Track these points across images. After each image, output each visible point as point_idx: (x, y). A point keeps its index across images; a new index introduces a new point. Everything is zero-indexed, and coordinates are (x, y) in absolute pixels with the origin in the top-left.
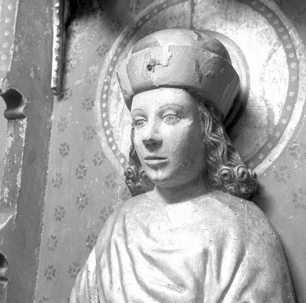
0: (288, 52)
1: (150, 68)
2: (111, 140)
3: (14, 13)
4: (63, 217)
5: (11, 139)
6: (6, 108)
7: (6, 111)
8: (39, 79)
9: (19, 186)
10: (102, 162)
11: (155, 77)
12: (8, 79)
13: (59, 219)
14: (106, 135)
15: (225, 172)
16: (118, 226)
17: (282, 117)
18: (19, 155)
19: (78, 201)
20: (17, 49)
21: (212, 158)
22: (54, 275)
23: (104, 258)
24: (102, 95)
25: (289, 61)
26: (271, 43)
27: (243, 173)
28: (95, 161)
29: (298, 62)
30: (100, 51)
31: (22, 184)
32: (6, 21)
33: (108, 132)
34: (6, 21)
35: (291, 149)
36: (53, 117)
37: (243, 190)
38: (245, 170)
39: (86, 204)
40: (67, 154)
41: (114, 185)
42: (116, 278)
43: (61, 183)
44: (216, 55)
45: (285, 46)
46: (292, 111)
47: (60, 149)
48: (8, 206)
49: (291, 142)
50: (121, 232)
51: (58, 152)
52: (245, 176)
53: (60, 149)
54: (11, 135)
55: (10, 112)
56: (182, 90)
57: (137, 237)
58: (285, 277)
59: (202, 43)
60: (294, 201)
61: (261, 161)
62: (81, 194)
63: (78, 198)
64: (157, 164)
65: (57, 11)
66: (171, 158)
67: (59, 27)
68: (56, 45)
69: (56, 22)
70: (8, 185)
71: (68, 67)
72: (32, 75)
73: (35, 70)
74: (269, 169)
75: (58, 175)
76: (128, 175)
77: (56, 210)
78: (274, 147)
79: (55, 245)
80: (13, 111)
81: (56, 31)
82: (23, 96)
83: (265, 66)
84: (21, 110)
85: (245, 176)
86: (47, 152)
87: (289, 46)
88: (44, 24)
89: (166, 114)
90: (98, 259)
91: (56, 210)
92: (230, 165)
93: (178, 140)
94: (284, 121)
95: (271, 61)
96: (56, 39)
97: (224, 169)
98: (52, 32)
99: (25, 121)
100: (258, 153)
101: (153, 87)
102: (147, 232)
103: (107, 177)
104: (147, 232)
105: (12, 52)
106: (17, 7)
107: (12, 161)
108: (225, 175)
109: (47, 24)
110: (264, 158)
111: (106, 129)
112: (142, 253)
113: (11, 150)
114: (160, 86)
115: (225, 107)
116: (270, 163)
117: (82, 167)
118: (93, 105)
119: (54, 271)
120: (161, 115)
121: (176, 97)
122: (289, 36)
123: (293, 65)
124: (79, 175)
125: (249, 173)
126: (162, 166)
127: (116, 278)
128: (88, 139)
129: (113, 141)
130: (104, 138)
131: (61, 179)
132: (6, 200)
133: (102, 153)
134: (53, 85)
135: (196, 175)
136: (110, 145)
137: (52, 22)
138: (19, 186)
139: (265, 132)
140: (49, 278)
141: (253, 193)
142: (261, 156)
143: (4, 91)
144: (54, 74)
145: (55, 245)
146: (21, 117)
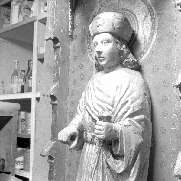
0: (151, 15)
1: (98, 26)
2: (91, 53)
3: (54, 8)
4: (76, 83)
5: (56, 56)
6: (53, 43)
7: (53, 45)
8: (65, 32)
9: (60, 72)
10: (88, 62)
11: (100, 30)
12: (53, 34)
13: (74, 84)
14: (89, 51)
15: (127, 61)
16: (91, 83)
17: (149, 40)
18: (59, 61)
19: (81, 77)
20: (56, 22)
21: (122, 56)
22: (74, 104)
23: (87, 92)
24: (88, 36)
25: (152, 19)
26: (146, 12)
27: (133, 61)
28: (86, 62)
29: (155, 19)
30: (86, 19)
31: (61, 72)
32: (52, 12)
33: (90, 50)
34: (52, 12)
35: (152, 51)
36: (71, 46)
37: (133, 67)
38: (133, 60)
39: (83, 78)
40: (76, 60)
41: (93, 70)
42: (90, 96)
43: (74, 71)
44: (119, 21)
45: (150, 14)
46: (152, 37)
47: (74, 58)
48: (56, 80)
49: (152, 49)
50: (92, 84)
51: (73, 59)
52: (133, 62)
53: (74, 58)
54: (56, 54)
55: (55, 46)
56: (108, 34)
57: (96, 84)
58: (145, 94)
59: (115, 16)
60: (153, 70)
61: (142, 56)
62: (81, 74)
63: (81, 76)
64: (102, 59)
65: (70, 6)
66: (106, 57)
67: (71, 12)
68: (70, 19)
69: (70, 10)
70: (56, 73)
71: (75, 27)
72: (62, 31)
73: (63, 29)
74: (145, 59)
75: (73, 68)
76: (96, 65)
77: (73, 81)
78: (146, 51)
79: (74, 94)
80: (77, 137)
81: (70, 13)
82: (59, 39)
83: (143, 21)
84: (58, 44)
85: (133, 62)
86: (69, 60)
87: (152, 13)
88: (66, 11)
89: (104, 42)
90: (85, 93)
91: (73, 81)
92: (128, 58)
93: (108, 50)
94: (150, 41)
95: (146, 19)
96: (70, 16)
97: (126, 60)
98: (69, 14)
99: (60, 48)
100: (141, 54)
101: (99, 33)
102: (99, 82)
103: (90, 67)
104: (99, 82)
105: (54, 24)
106: (55, 7)
107: (56, 64)
108: (126, 62)
109: (67, 11)
110: (143, 55)
111: (89, 49)
112: (98, 89)
113: (56, 60)
114: (102, 33)
115: (127, 37)
116: (145, 57)
117: (81, 64)
118: (84, 40)
119: (74, 103)
120: (102, 42)
121: (109, 36)
122: (152, 9)
123: (153, 20)
124: (80, 67)
125: (135, 61)
126: (104, 60)
127: (90, 96)
128: (83, 54)
129: (92, 54)
130: (89, 53)
131: (75, 69)
132: (55, 78)
133: (88, 59)
134: (70, 34)
135: (117, 61)
136: (91, 55)
137: (68, 10)
138: (60, 72)
139: (143, 46)
140: (72, 105)
141: (138, 68)
142: (142, 55)
143: (52, 38)
144: (70, 30)
145: (74, 94)
146: (59, 47)
